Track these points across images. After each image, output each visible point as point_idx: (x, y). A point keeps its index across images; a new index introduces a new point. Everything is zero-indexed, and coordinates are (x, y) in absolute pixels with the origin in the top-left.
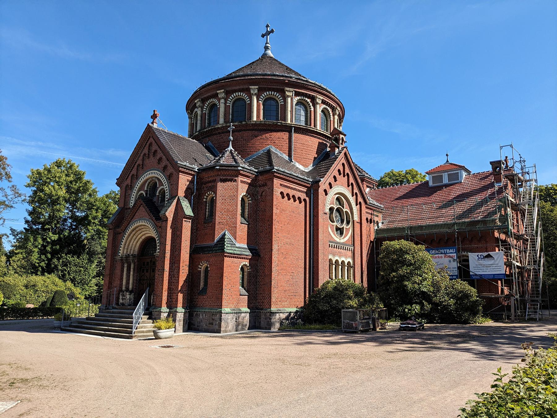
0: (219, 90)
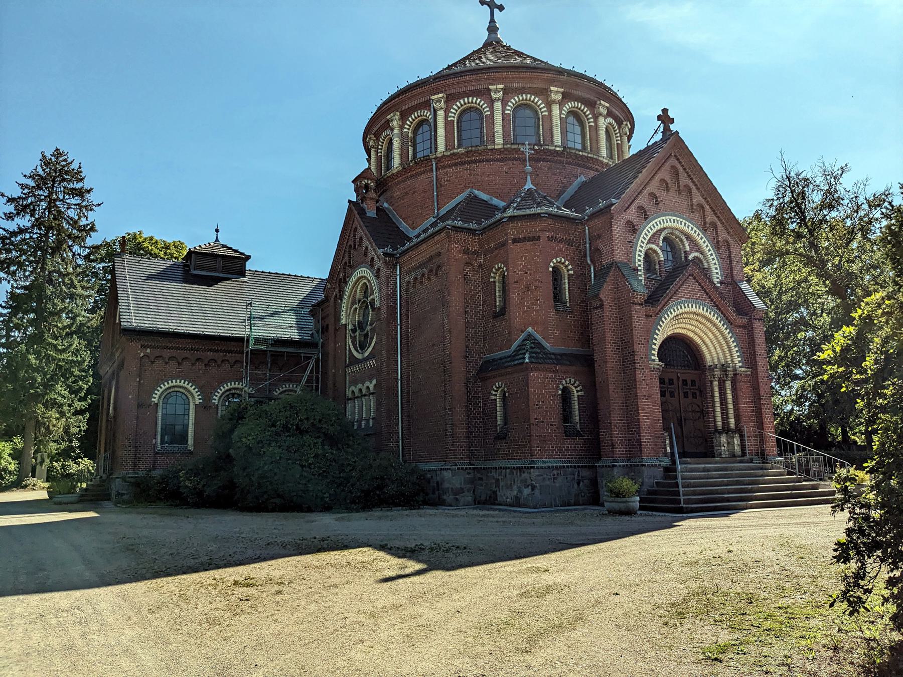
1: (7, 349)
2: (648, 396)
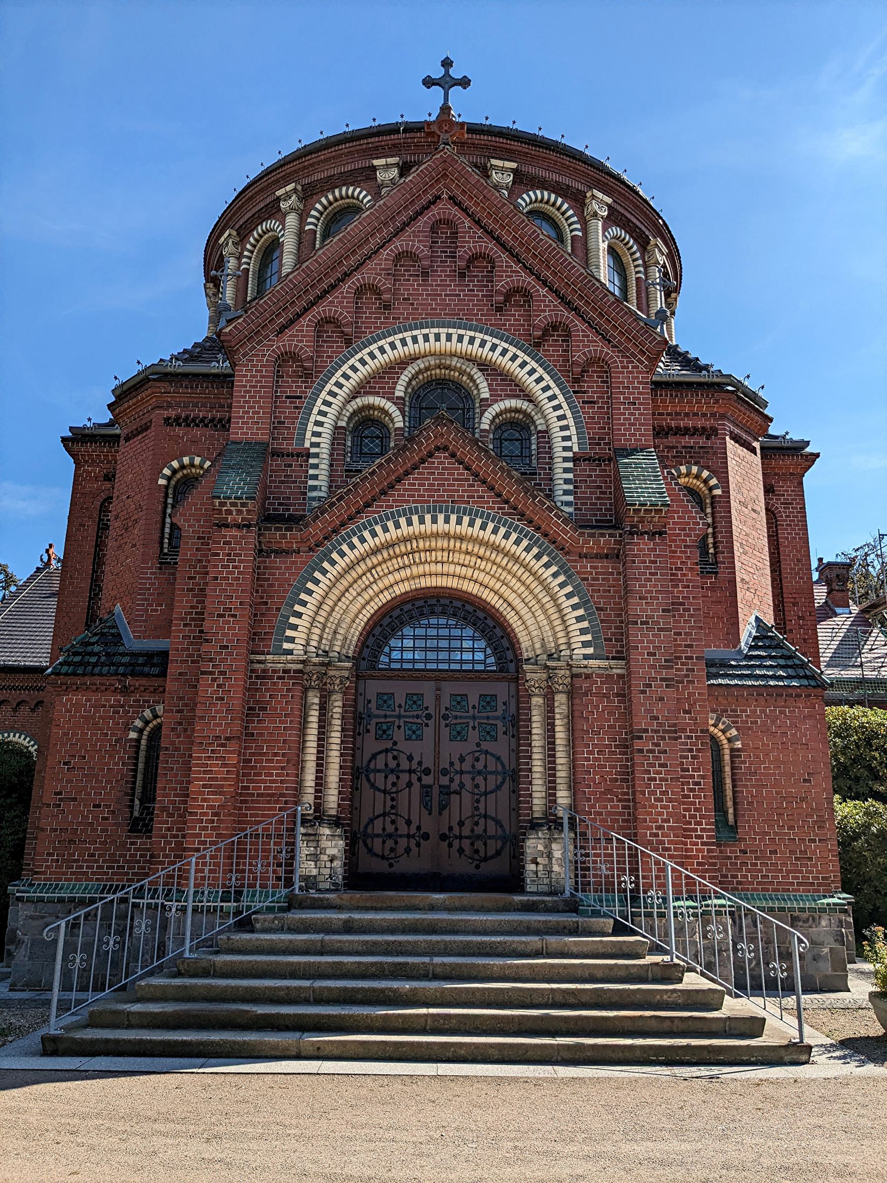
0: (377, 158)
2: (227, 739)
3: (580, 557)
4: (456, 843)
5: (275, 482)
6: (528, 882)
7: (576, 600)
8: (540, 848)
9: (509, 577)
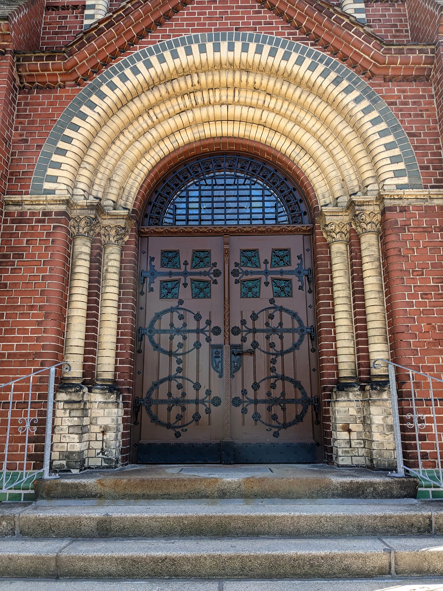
1: (36, 461)
3: (385, 80)
4: (251, 408)
5: (49, 33)
6: (340, 453)
7: (383, 126)
8: (353, 412)
9: (302, 114)
